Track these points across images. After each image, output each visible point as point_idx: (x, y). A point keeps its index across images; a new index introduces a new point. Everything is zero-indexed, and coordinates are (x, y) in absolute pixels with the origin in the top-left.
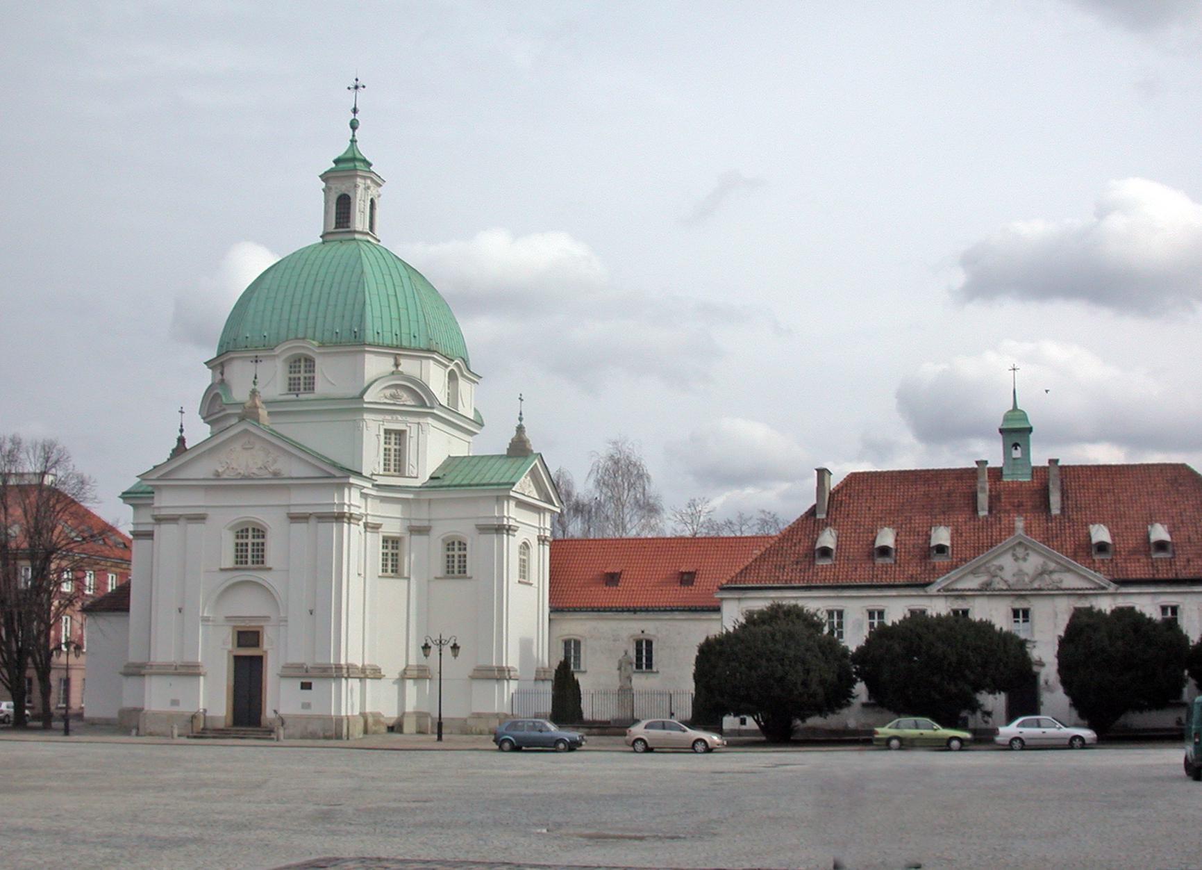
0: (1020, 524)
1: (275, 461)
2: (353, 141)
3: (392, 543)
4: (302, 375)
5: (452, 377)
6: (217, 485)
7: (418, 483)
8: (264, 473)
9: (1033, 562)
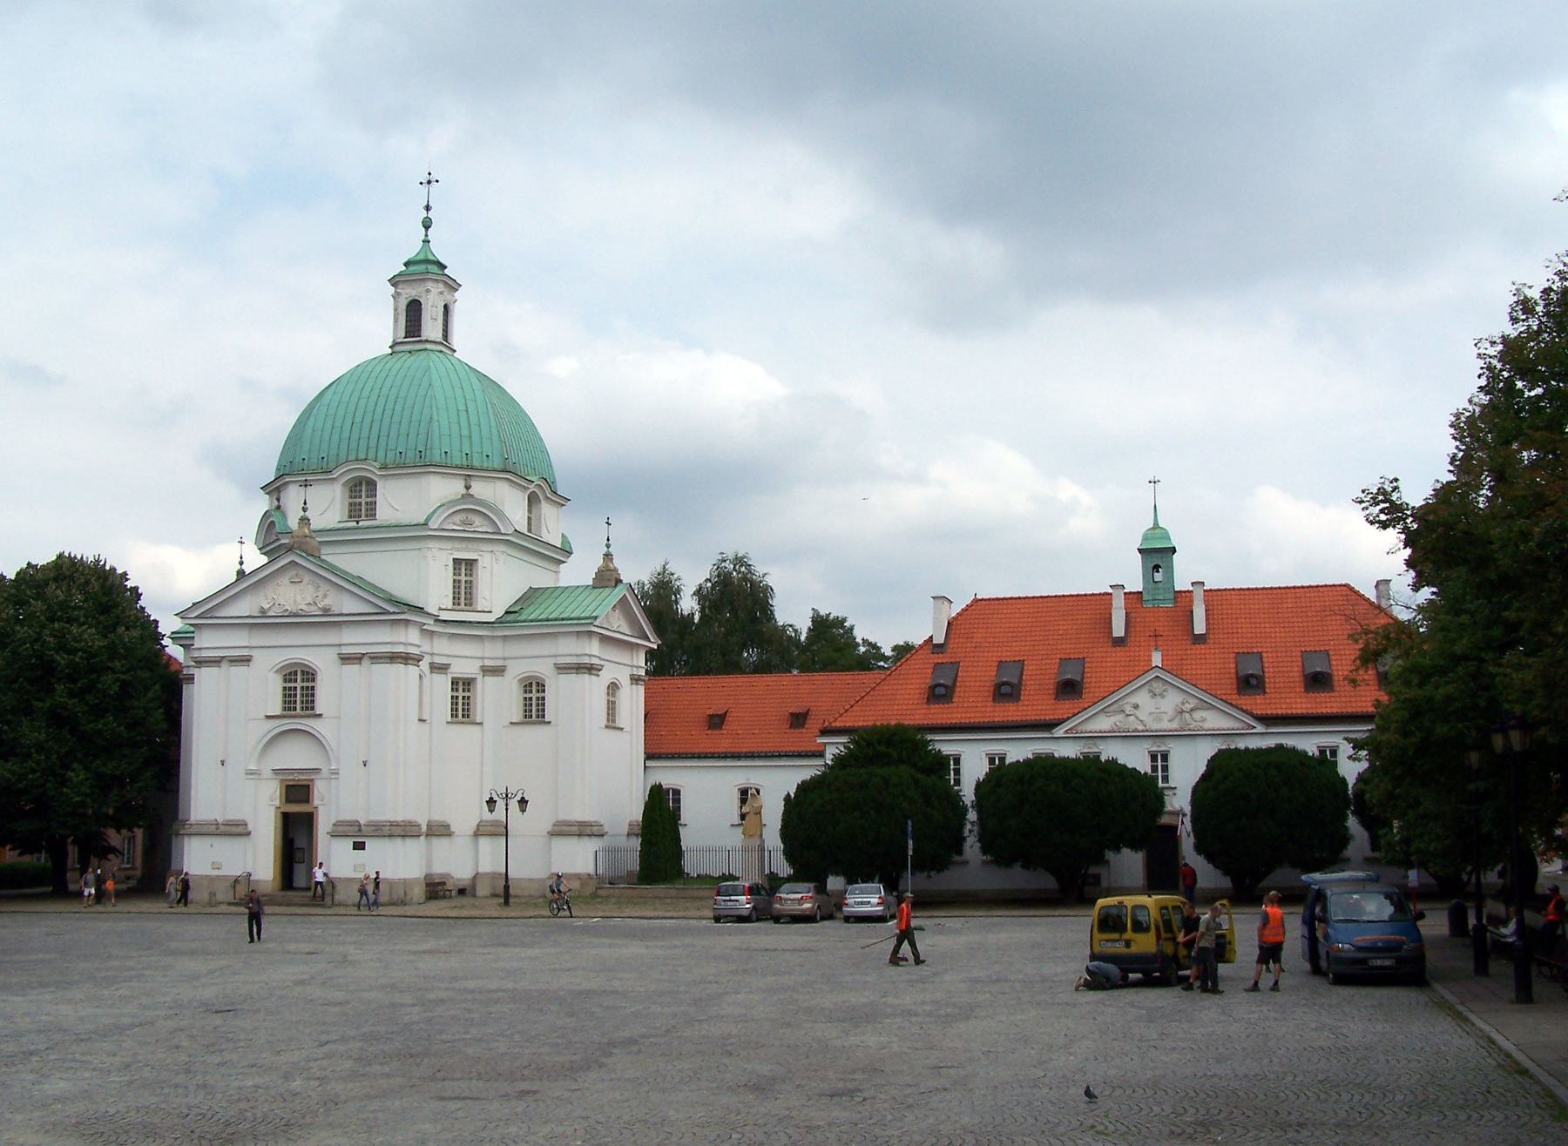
0: (1157, 659)
1: (325, 596)
2: (426, 242)
3: (463, 685)
4: (363, 500)
5: (533, 500)
6: (262, 623)
8: (313, 610)
9: (1171, 701)
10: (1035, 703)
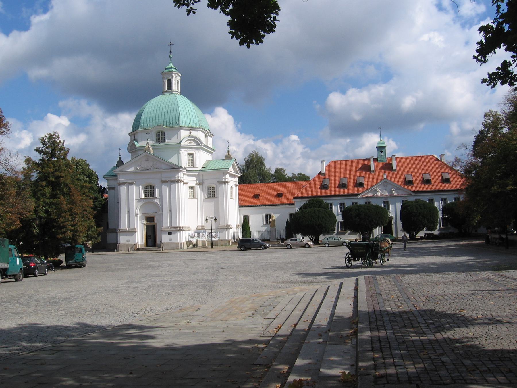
4: (161, 137)
5: (206, 136)
7: (198, 169)
10: (351, 189)
